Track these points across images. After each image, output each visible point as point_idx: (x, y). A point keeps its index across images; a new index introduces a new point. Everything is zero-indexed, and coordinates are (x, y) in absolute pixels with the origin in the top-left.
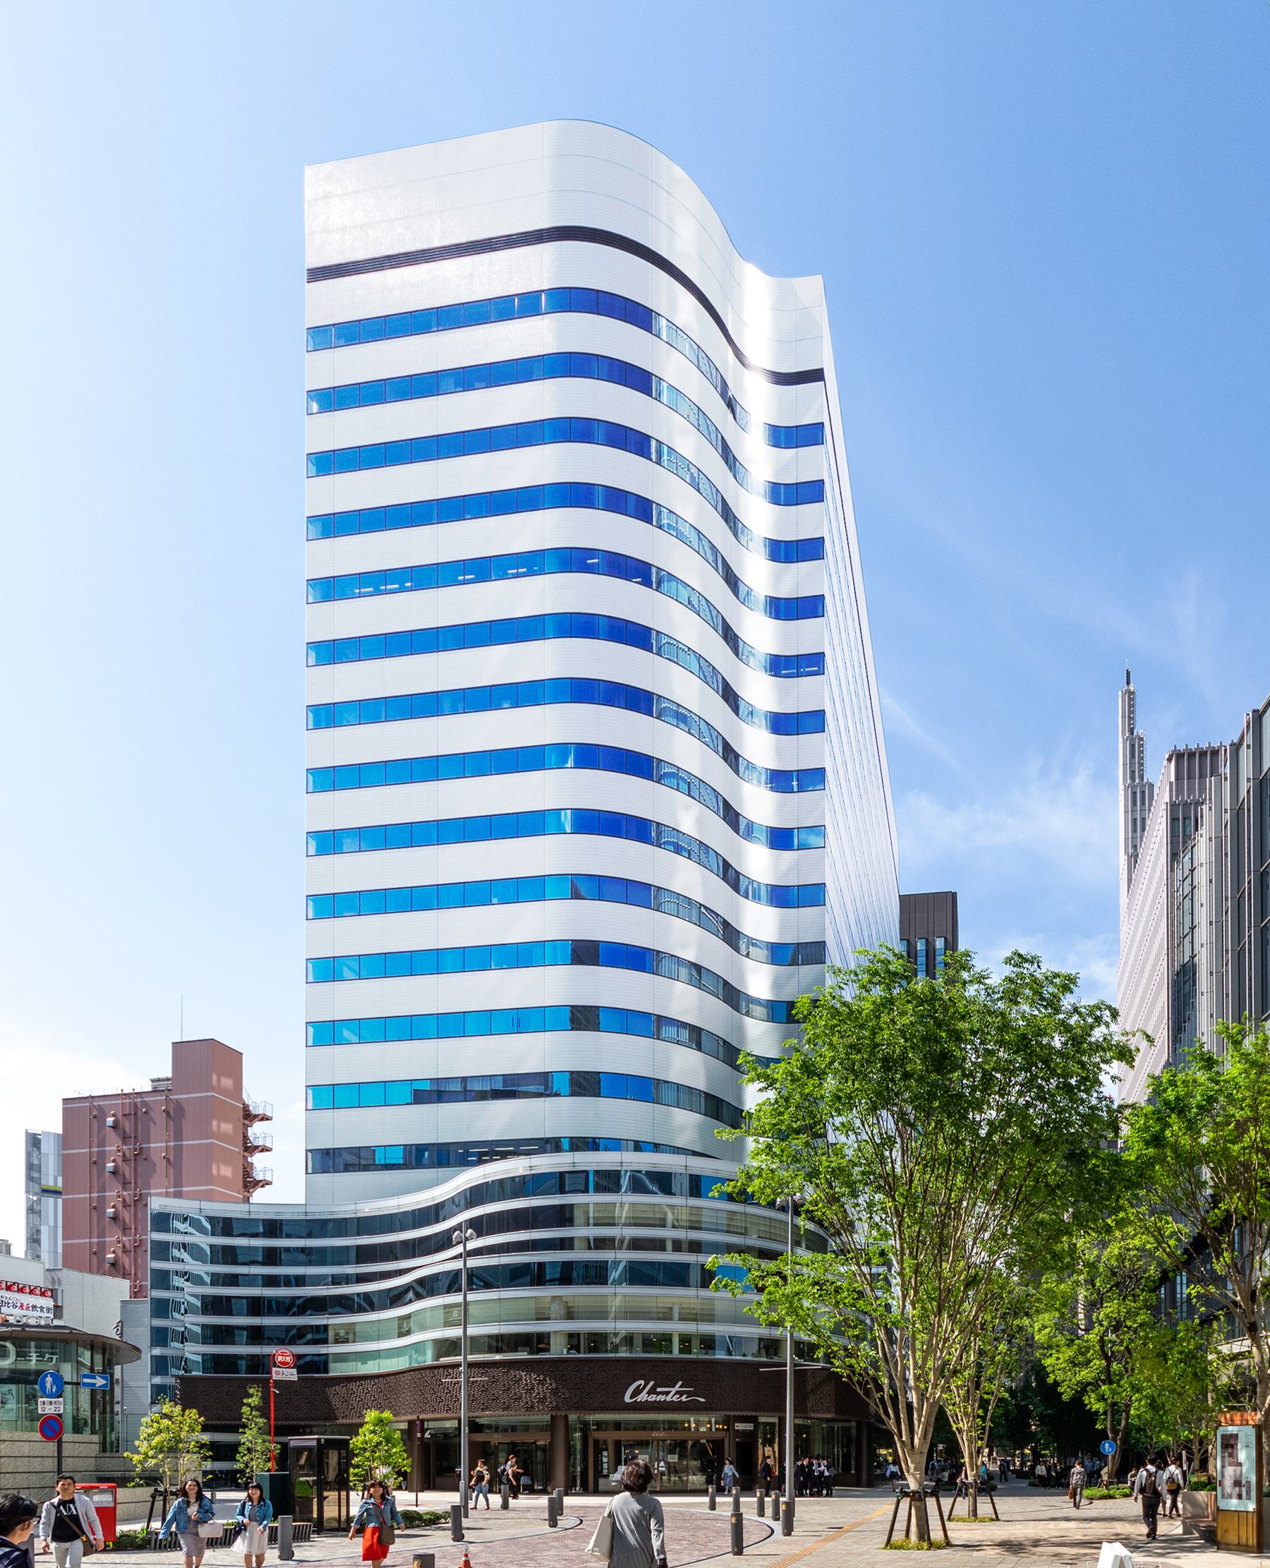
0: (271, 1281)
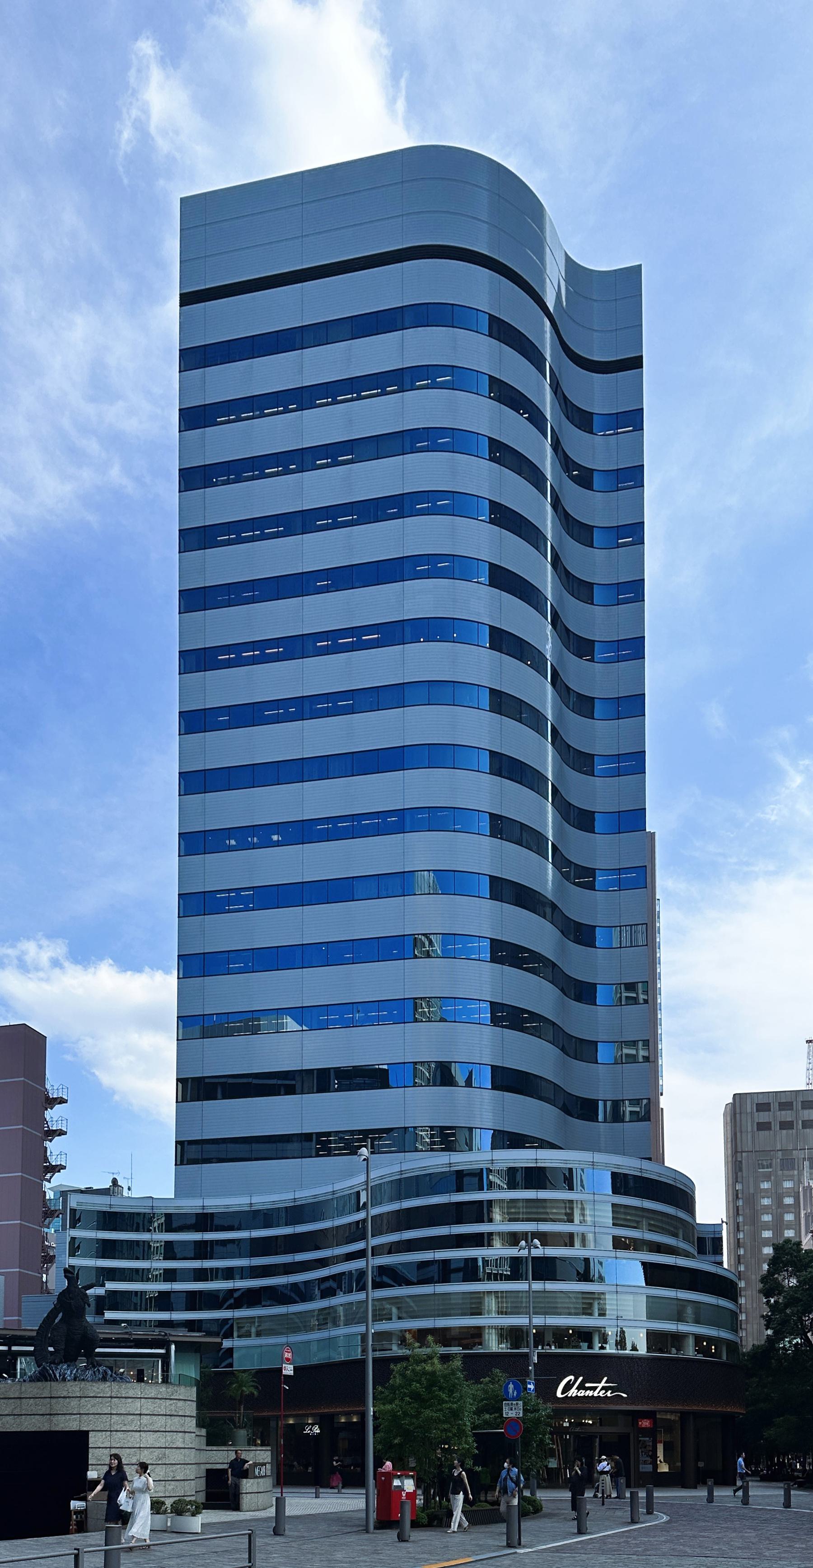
0: (201, 1275)
